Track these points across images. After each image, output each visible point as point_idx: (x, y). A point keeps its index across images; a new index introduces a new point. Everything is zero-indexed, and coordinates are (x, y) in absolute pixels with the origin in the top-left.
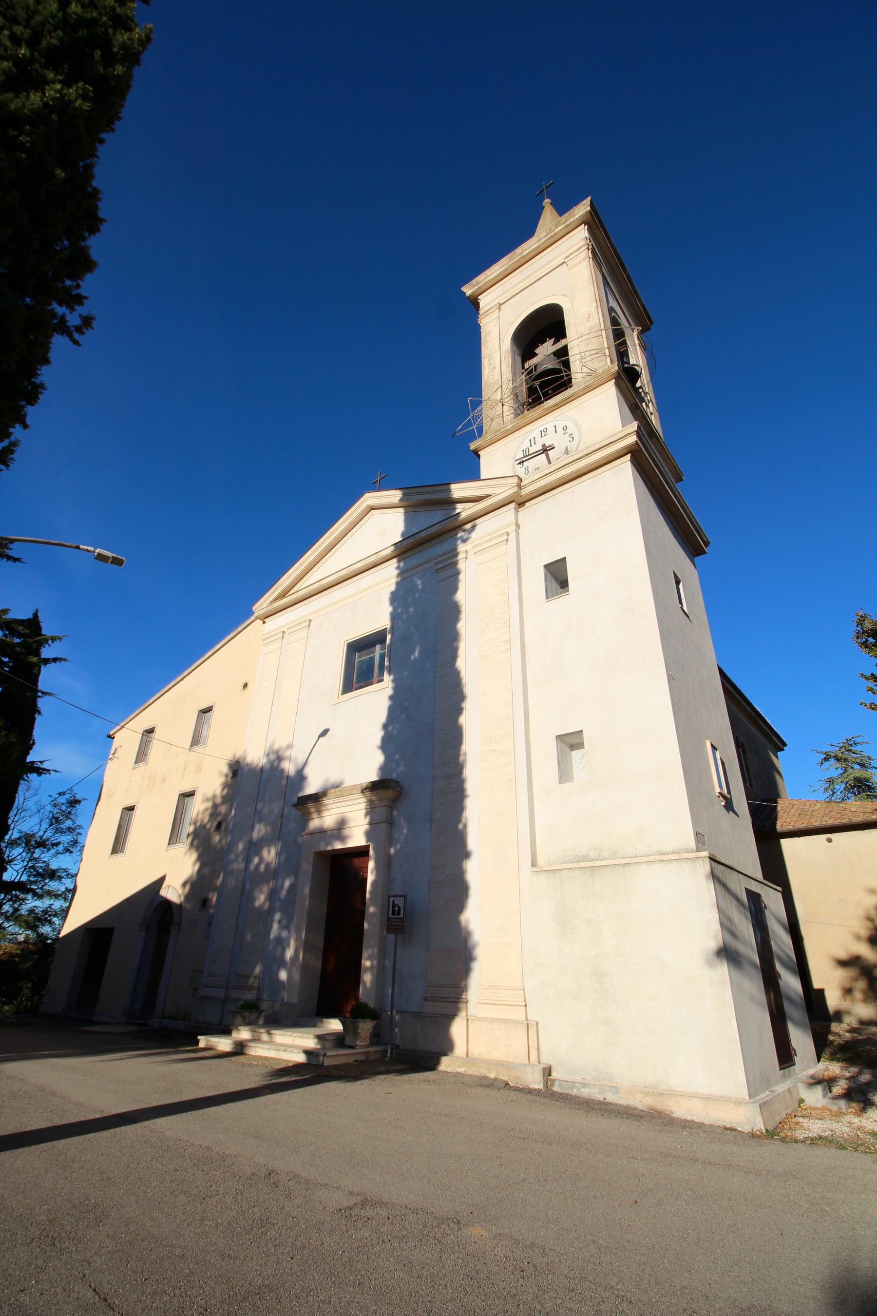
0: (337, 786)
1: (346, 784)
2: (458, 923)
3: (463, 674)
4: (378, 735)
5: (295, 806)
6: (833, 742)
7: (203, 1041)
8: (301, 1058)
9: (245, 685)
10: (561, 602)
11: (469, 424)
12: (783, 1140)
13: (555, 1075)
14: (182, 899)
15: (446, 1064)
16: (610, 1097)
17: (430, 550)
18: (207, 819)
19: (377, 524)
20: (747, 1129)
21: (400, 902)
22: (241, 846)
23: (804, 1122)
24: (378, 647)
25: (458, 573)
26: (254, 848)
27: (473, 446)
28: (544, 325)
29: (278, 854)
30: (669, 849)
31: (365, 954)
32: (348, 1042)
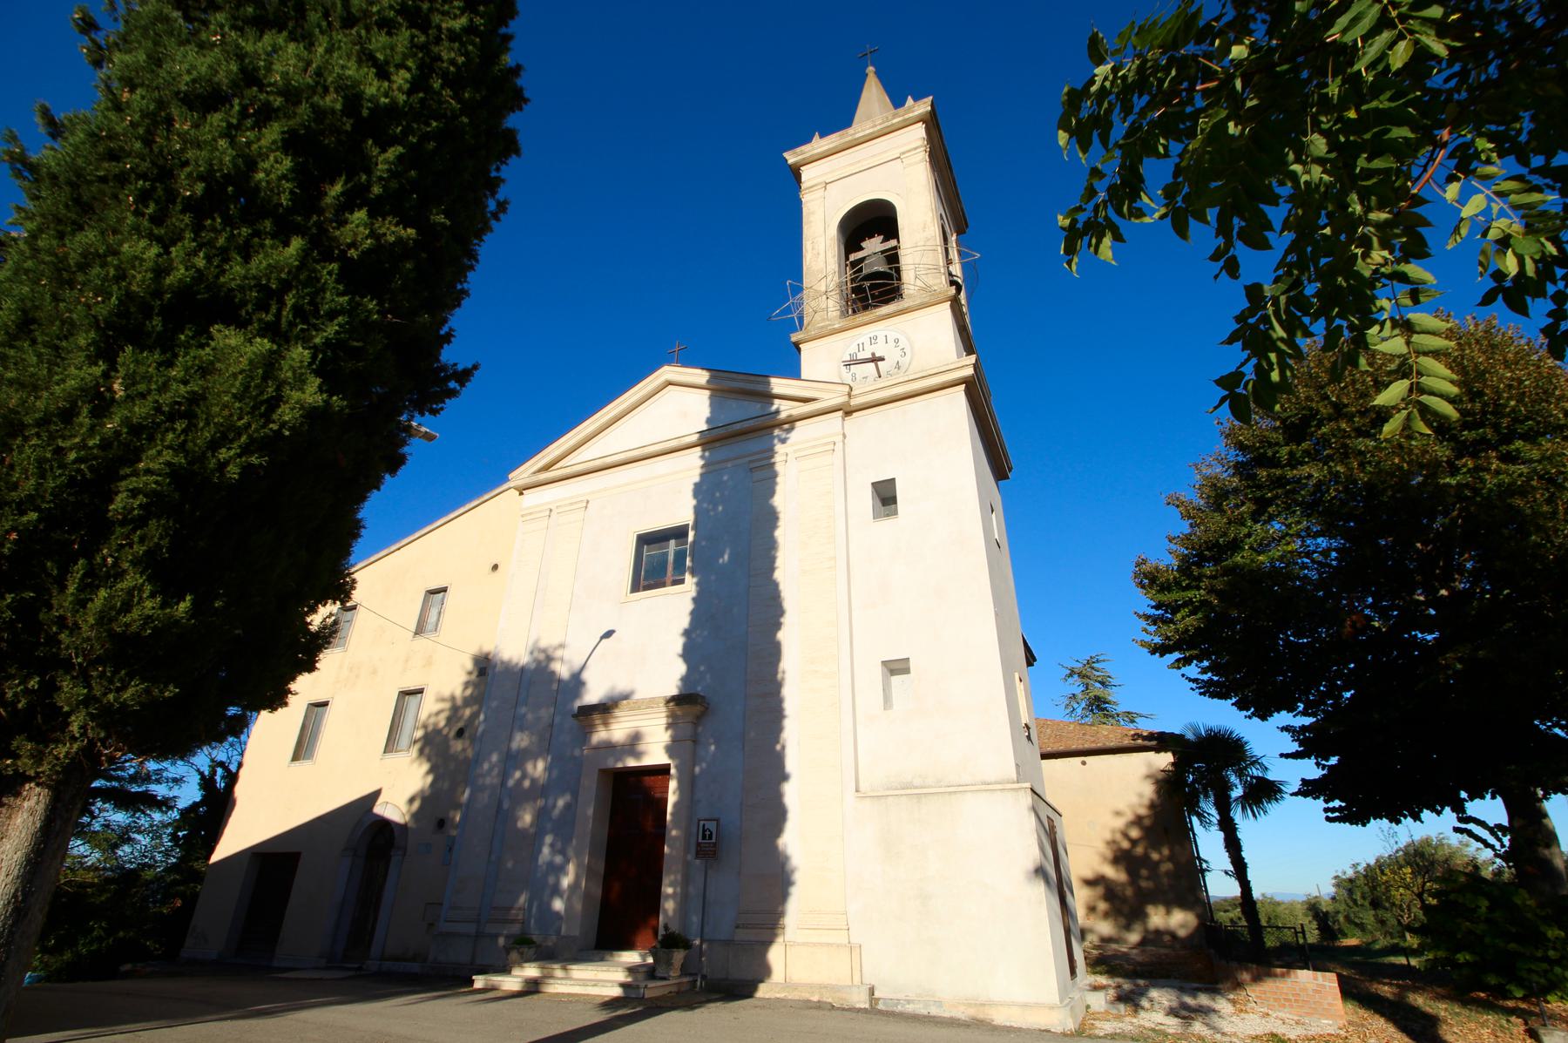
0: (626, 697)
1: (637, 696)
2: (775, 847)
3: (782, 587)
4: (678, 644)
5: (575, 716)
6: (1076, 659)
7: (479, 982)
8: (617, 992)
9: (495, 567)
10: (887, 524)
11: (788, 310)
12: (1089, 1036)
13: (877, 994)
14: (407, 818)
15: (763, 991)
16: (934, 1011)
17: (741, 445)
18: (442, 723)
19: (675, 405)
20: (1059, 1029)
21: (712, 826)
22: (495, 758)
23: (1097, 1024)
24: (672, 542)
25: (775, 475)
26: (514, 760)
27: (794, 338)
28: (871, 221)
29: (548, 769)
30: (993, 779)
31: (666, 880)
32: (660, 973)
